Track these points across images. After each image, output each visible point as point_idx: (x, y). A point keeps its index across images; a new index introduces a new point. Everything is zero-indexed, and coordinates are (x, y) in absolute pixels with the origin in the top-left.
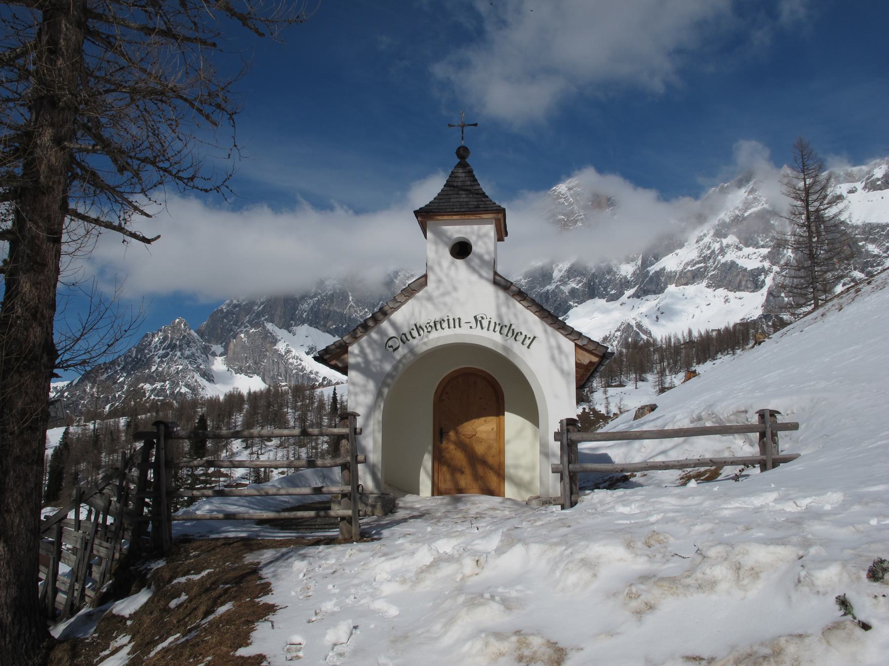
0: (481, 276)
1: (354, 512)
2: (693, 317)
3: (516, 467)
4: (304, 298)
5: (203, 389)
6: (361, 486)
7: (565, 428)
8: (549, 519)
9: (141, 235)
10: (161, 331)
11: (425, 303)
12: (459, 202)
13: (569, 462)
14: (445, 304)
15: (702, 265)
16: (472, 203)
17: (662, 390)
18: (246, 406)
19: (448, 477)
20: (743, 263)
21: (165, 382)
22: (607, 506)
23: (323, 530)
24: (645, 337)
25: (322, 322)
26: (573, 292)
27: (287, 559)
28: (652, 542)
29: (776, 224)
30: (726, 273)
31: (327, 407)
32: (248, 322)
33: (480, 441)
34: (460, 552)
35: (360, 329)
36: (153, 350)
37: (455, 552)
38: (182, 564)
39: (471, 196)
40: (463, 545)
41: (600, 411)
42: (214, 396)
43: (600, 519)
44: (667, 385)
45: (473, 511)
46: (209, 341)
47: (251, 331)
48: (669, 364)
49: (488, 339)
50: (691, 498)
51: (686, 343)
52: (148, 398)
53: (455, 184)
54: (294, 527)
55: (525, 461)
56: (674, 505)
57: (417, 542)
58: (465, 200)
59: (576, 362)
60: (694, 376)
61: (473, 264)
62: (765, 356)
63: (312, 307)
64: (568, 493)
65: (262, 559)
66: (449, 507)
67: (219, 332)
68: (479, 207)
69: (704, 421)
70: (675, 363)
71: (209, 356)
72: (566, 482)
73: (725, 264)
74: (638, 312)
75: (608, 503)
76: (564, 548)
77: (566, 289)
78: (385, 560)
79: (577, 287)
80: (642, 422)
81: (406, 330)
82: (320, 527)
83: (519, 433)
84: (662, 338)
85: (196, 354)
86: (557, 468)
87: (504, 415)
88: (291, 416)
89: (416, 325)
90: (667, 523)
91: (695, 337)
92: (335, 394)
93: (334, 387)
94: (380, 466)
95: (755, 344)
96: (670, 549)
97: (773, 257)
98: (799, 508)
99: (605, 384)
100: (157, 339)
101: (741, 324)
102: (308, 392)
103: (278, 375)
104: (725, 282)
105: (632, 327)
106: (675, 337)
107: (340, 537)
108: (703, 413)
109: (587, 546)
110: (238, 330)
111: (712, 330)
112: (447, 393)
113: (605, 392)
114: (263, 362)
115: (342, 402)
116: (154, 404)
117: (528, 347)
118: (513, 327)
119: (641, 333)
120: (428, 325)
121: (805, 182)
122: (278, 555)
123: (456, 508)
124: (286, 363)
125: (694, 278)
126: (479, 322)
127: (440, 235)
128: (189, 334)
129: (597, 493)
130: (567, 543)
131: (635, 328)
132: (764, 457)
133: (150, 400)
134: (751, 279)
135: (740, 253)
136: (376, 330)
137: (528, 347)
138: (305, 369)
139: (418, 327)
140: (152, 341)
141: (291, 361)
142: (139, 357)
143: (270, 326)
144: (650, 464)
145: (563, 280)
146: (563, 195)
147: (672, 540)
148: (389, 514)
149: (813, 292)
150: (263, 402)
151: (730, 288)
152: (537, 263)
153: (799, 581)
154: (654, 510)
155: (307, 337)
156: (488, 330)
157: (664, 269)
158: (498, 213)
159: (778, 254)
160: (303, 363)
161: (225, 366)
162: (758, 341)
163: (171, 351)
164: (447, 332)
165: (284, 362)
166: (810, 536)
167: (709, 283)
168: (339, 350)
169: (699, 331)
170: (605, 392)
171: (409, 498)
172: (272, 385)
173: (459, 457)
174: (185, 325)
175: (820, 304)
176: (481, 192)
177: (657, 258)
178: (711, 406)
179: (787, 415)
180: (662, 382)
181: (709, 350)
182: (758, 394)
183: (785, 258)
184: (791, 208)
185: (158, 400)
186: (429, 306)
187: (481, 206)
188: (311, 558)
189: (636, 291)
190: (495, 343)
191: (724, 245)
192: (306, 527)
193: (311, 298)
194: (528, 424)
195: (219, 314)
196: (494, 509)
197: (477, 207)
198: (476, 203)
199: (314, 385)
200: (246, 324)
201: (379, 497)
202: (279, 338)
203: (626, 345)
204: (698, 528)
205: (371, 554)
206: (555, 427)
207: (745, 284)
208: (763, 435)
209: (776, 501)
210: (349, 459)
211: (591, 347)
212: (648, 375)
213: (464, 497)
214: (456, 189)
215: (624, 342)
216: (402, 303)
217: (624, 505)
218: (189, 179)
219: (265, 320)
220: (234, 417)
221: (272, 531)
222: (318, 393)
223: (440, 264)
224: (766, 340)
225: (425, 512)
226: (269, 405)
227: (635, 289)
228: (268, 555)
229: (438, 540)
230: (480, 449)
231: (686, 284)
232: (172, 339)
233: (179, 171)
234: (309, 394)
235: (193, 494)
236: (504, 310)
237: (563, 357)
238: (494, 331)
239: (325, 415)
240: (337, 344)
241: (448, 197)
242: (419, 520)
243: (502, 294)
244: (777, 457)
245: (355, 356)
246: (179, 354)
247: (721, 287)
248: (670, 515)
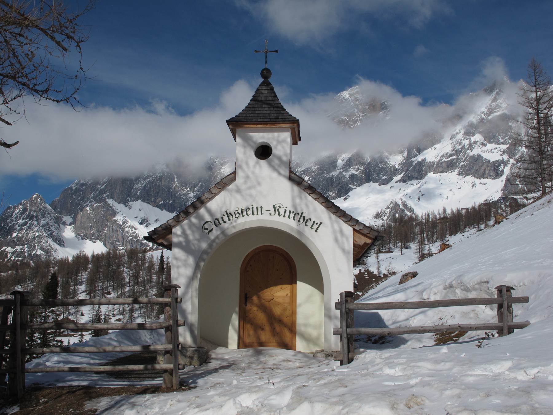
0: (280, 174)
1: (175, 366)
2: (447, 198)
3: (306, 325)
4: (138, 179)
5: (55, 251)
6: (180, 345)
7: (344, 299)
8: (330, 378)
9: (2, 141)
10: (21, 204)
12: (262, 113)
13: (347, 327)
14: (251, 196)
15: (455, 157)
16: (273, 115)
17: (422, 257)
18: (90, 266)
19: (252, 332)
20: (486, 156)
21: (23, 245)
22: (376, 368)
23: (150, 379)
24: (409, 214)
25: (153, 199)
26: (353, 177)
27: (119, 407)
28: (412, 404)
29: (513, 125)
30: (474, 164)
31: (156, 267)
32: (93, 198)
33: (278, 304)
34: (258, 407)
35: (182, 214)
36: (14, 220)
37: (255, 408)
38: (32, 410)
39: (272, 109)
40: (261, 400)
41: (373, 272)
42: (64, 257)
43: (370, 380)
44: (426, 252)
45: (271, 362)
46: (61, 213)
47: (95, 205)
48: (427, 235)
50: (443, 364)
51: (441, 219)
52: (10, 259)
53: (260, 99)
54: (126, 376)
55: (312, 321)
56: (429, 370)
57: (225, 395)
58: (268, 112)
59: (354, 243)
60: (447, 248)
61: (273, 163)
62: (503, 234)
63: (145, 186)
64: (346, 351)
65: (99, 406)
66: (252, 359)
67: (69, 205)
68: (279, 118)
69: (454, 288)
70: (433, 235)
71: (60, 225)
72: (344, 343)
73: (472, 157)
74: (403, 194)
75: (378, 364)
76: (341, 407)
77: (347, 175)
78: (198, 412)
79: (356, 173)
80: (405, 287)
81: (219, 216)
82: (148, 375)
83: (309, 299)
84: (422, 215)
85: (50, 224)
86: (337, 331)
87: (296, 283)
88: (127, 274)
89: (226, 212)
90: (424, 386)
91: (449, 214)
92: (162, 256)
93: (161, 251)
94: (196, 325)
95: (495, 223)
96: (425, 410)
97: (511, 152)
98: (528, 376)
99: (377, 250)
100: (18, 211)
101: (485, 204)
102: (141, 255)
103: (116, 241)
104: (473, 171)
105: (398, 205)
106: (433, 213)
107: (164, 386)
108: (454, 282)
109: (360, 407)
110: (85, 205)
111: (462, 209)
112: (251, 266)
113: (377, 257)
114: (105, 230)
115: (168, 263)
116: (15, 263)
117: (316, 231)
118: (304, 215)
119: (406, 211)
120: (236, 212)
121: (536, 94)
122: (113, 402)
123: (258, 360)
124: (123, 231)
125: (448, 167)
126: (277, 210)
127: (247, 140)
128: (45, 207)
129: (369, 354)
130: (344, 403)
131: (401, 207)
132: (501, 324)
133: (11, 260)
134: (493, 169)
135: (485, 148)
136: (194, 215)
137: (316, 231)
138: (138, 236)
139: (228, 213)
140: (14, 212)
141: (127, 229)
142: (3, 225)
143: (110, 201)
144: (411, 329)
145: (345, 167)
146: (346, 100)
147: (427, 402)
148: (203, 364)
149: (541, 182)
150: (104, 263)
151: (476, 175)
152: (325, 154)
154: (414, 374)
155: (140, 210)
156: (284, 216)
157: (424, 160)
158: (293, 123)
159: (515, 149)
160: (137, 232)
161: (74, 233)
162: (498, 221)
163: (29, 221)
164: (252, 218)
165: (122, 230)
166: (537, 405)
167: (460, 172)
168: (165, 231)
169: (452, 209)
170: (377, 257)
171: (220, 351)
172: (111, 249)
173: (261, 317)
174: (41, 200)
175: (547, 191)
176: (280, 106)
177: (419, 151)
178: (460, 276)
179: (520, 286)
180: (422, 250)
181: (459, 225)
182: (497, 268)
183: (520, 153)
184: (525, 114)
185: (18, 261)
186: (238, 197)
187: (280, 117)
188: (139, 407)
189: (402, 177)
190: (292, 228)
191: (472, 141)
192: (136, 376)
193: (144, 179)
194: (316, 291)
195: (69, 191)
196: (287, 361)
198: (276, 115)
199: (146, 249)
200: (91, 199)
201: (195, 350)
202: (117, 211)
203: (394, 220)
204: (448, 393)
205: (188, 404)
206: (336, 298)
207: (489, 173)
208: (500, 307)
209: (510, 369)
210: (171, 322)
211: (366, 231)
212: (411, 244)
213: (264, 350)
214: (260, 103)
215: (393, 217)
216: (216, 194)
217: (390, 368)
218: (43, 91)
219: (106, 196)
220: (80, 275)
221: (108, 379)
222: (148, 256)
223: (247, 164)
224: (504, 220)
225: (232, 362)
226: (109, 265)
227: (402, 175)
228: (104, 402)
229: (241, 394)
230: (277, 311)
231: (442, 172)
232: (30, 210)
233: (35, 85)
234: (142, 256)
235: (43, 351)
237: (344, 239)
238: (289, 217)
239: (154, 274)
240: (163, 226)
241: (254, 109)
242: (227, 370)
243: (296, 188)
244: (512, 324)
246: (35, 223)
247: (469, 175)
248: (427, 379)
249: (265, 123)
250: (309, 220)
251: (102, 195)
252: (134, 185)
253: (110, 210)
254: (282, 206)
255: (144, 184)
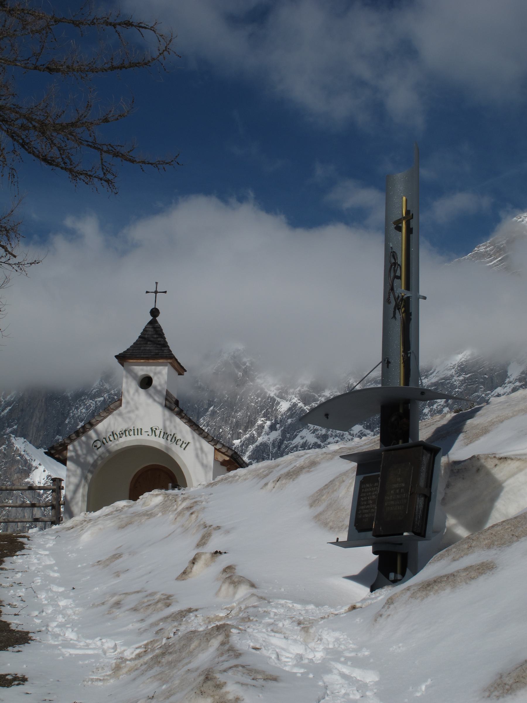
0: (155, 400)
11: (117, 417)
14: (130, 418)
49: (156, 442)
68: (158, 355)
117: (184, 449)
126: (153, 432)
137: (184, 449)
153: (354, 608)
156: (159, 437)
164: (129, 438)
186: (120, 419)
187: (160, 354)
197: (157, 354)
198: (157, 351)
216: (105, 417)
219: (12, 432)
236: (168, 423)
237: (204, 455)
245: (71, 451)
249: (148, 358)
250: (179, 440)
251: (3, 429)
252: (71, 409)
253: (18, 461)
254: (158, 429)
255: (93, 407)
